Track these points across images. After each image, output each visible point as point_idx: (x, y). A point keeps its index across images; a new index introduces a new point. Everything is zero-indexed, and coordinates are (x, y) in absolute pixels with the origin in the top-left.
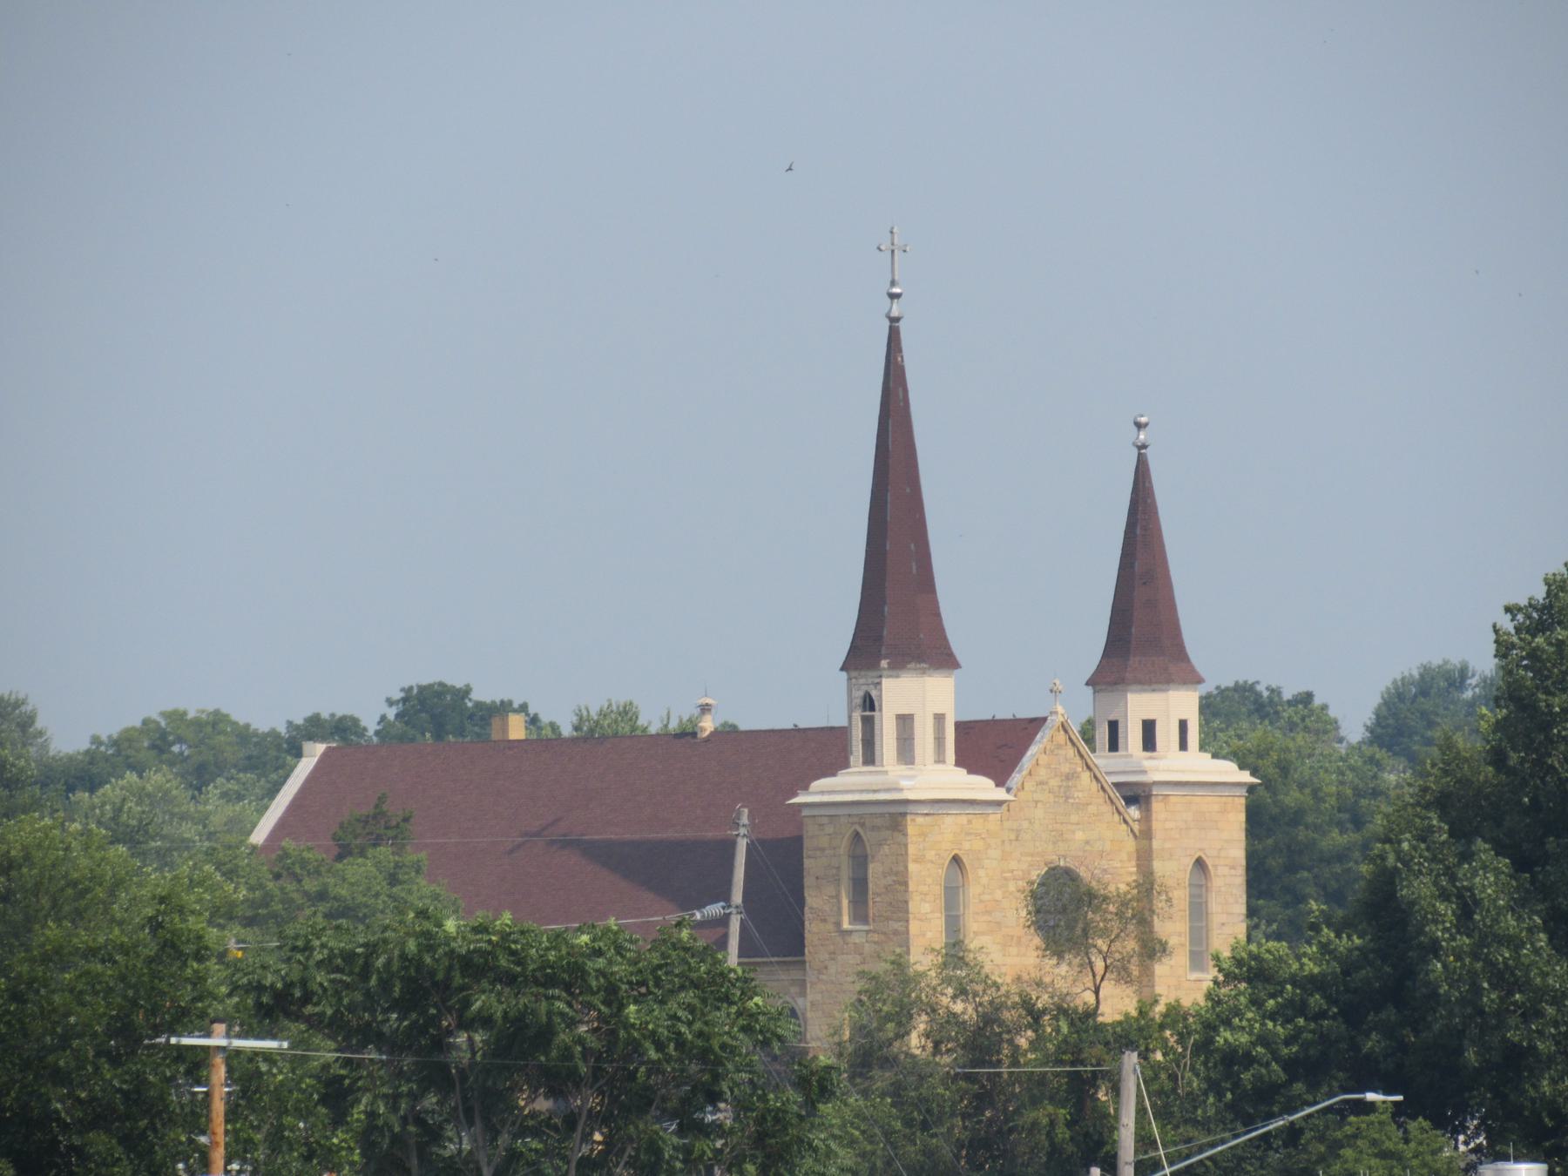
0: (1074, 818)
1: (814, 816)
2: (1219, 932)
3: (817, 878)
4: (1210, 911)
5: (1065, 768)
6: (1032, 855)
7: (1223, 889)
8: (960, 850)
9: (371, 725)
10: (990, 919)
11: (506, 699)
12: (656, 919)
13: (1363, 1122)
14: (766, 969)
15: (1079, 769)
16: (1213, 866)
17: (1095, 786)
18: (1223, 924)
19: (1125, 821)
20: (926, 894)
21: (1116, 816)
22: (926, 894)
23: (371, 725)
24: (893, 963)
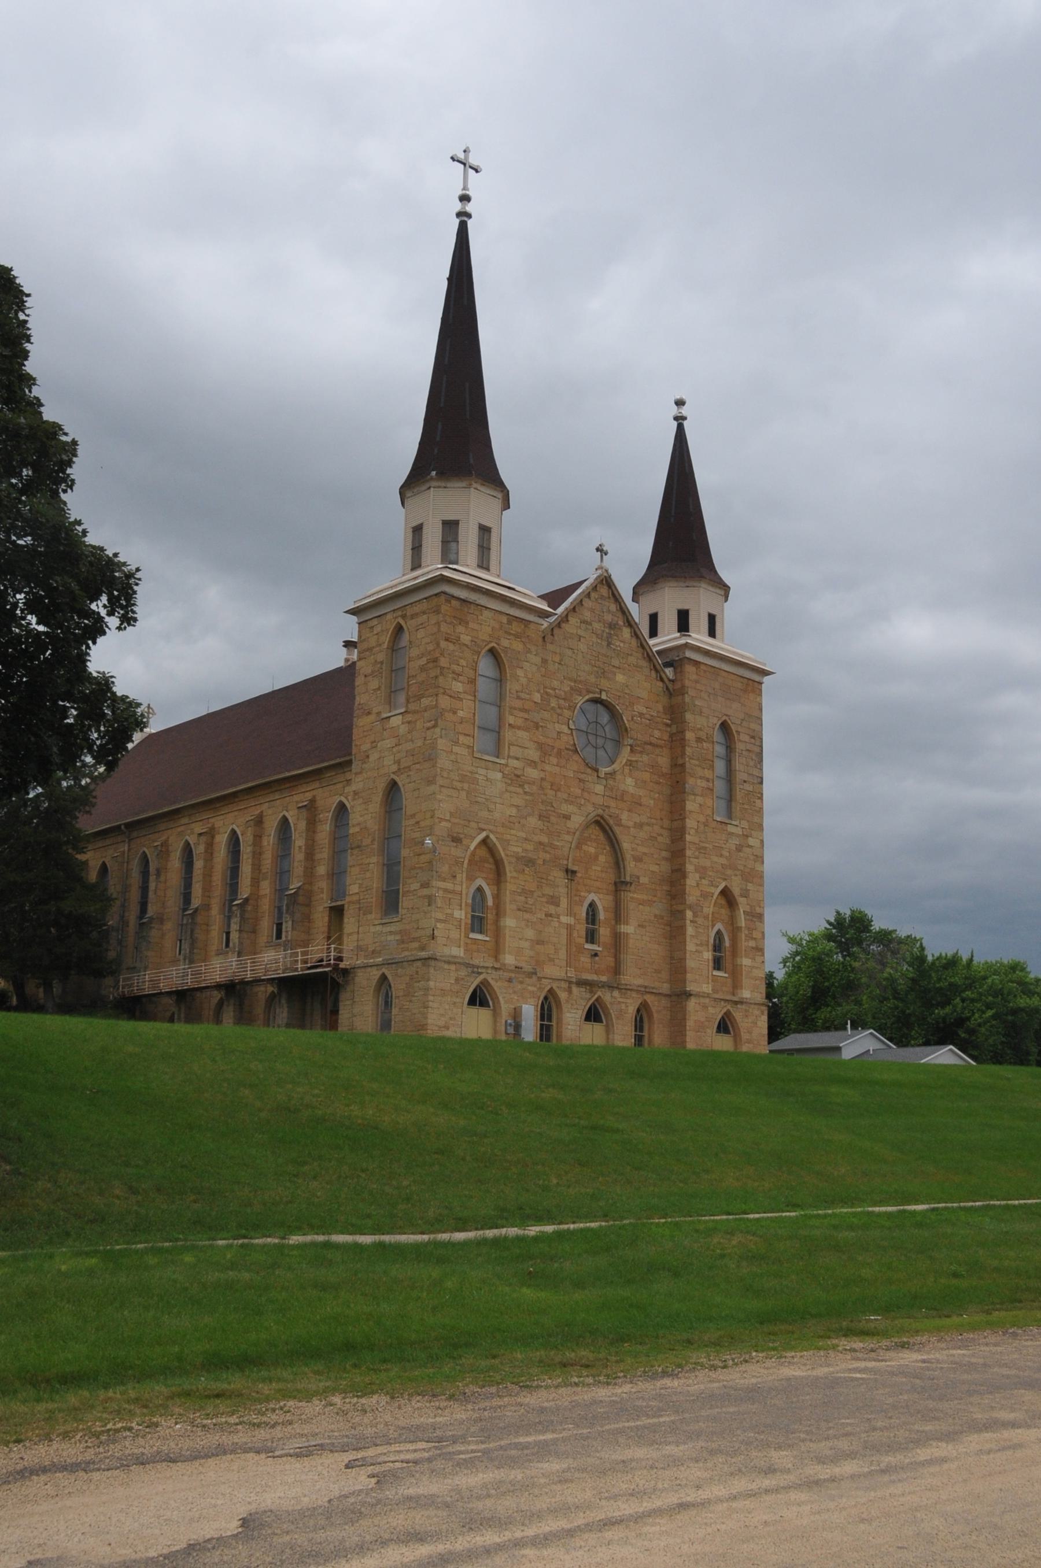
0: (616, 662)
1: (367, 621)
2: (742, 787)
3: (366, 676)
4: (733, 769)
5: (608, 618)
6: (575, 681)
7: (744, 752)
8: (498, 645)
9: (86, 539)
10: (526, 716)
11: (28, 325)
12: (757, 1216)
13: (556, 951)
14: (932, 1469)
15: (621, 623)
16: (737, 731)
17: (634, 642)
18: (745, 782)
19: (662, 680)
20: (459, 675)
21: (653, 672)
22: (459, 675)
23: (86, 539)
24: (394, 763)
